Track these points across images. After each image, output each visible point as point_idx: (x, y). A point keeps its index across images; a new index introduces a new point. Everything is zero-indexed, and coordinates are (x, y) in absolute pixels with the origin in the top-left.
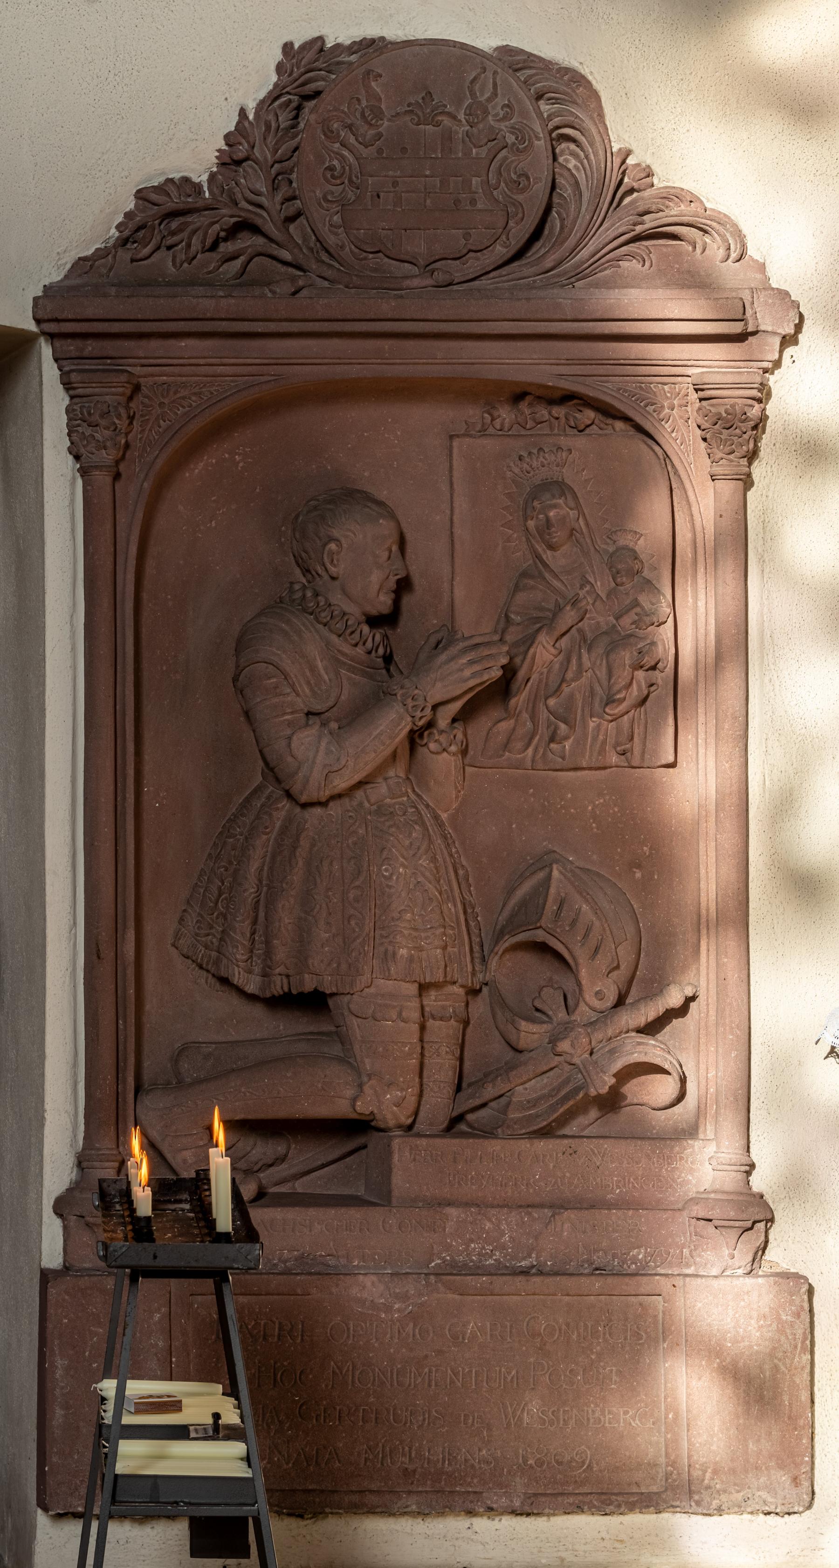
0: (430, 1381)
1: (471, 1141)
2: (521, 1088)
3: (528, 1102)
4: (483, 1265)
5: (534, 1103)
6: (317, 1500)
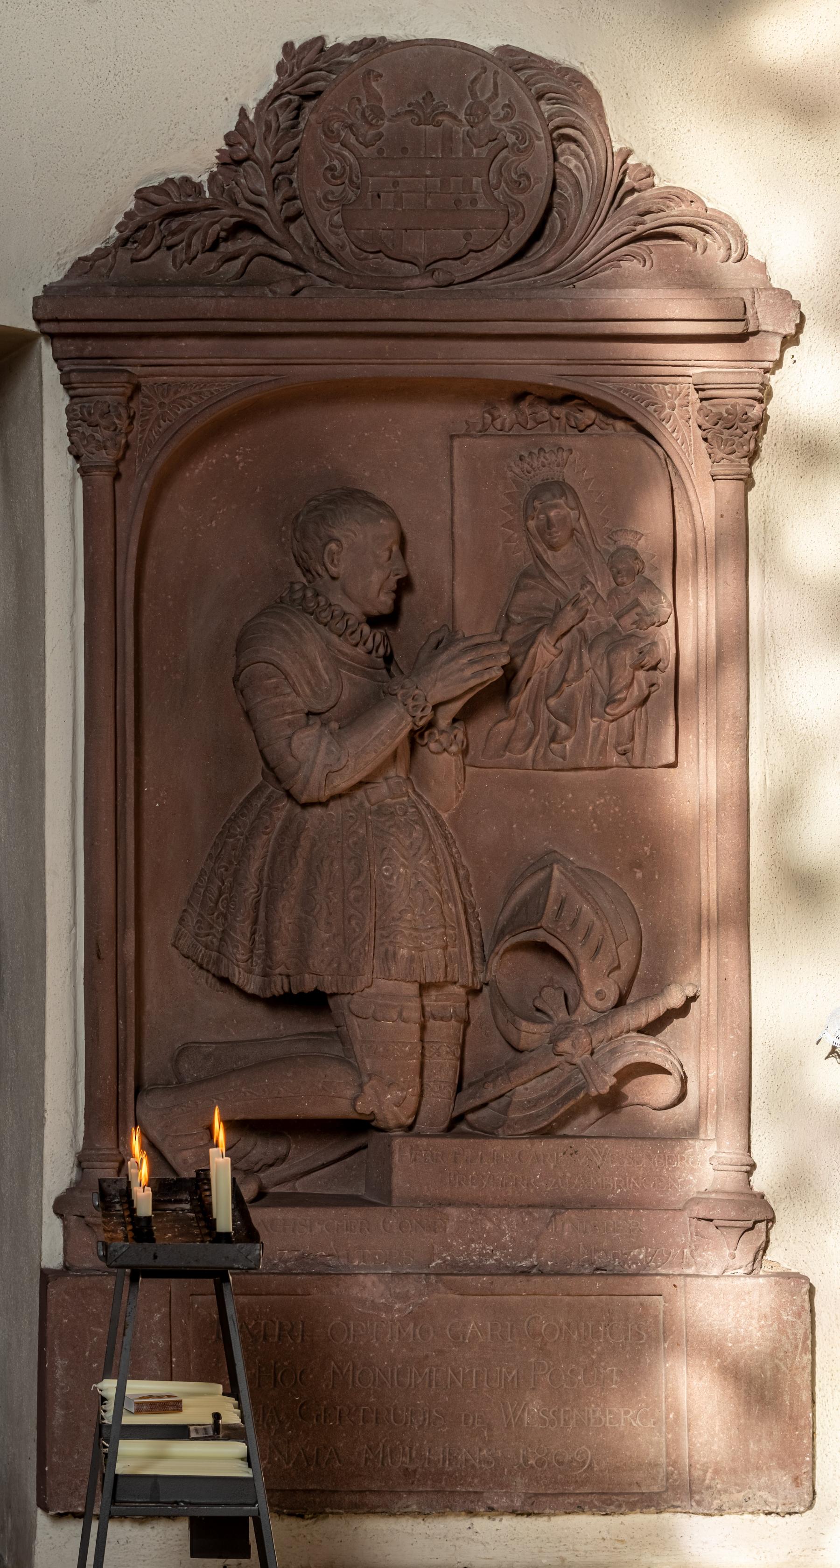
0: (430, 1381)
1: (471, 1141)
2: (521, 1088)
3: (529, 1102)
4: (484, 1265)
5: (534, 1103)
6: (318, 1500)
